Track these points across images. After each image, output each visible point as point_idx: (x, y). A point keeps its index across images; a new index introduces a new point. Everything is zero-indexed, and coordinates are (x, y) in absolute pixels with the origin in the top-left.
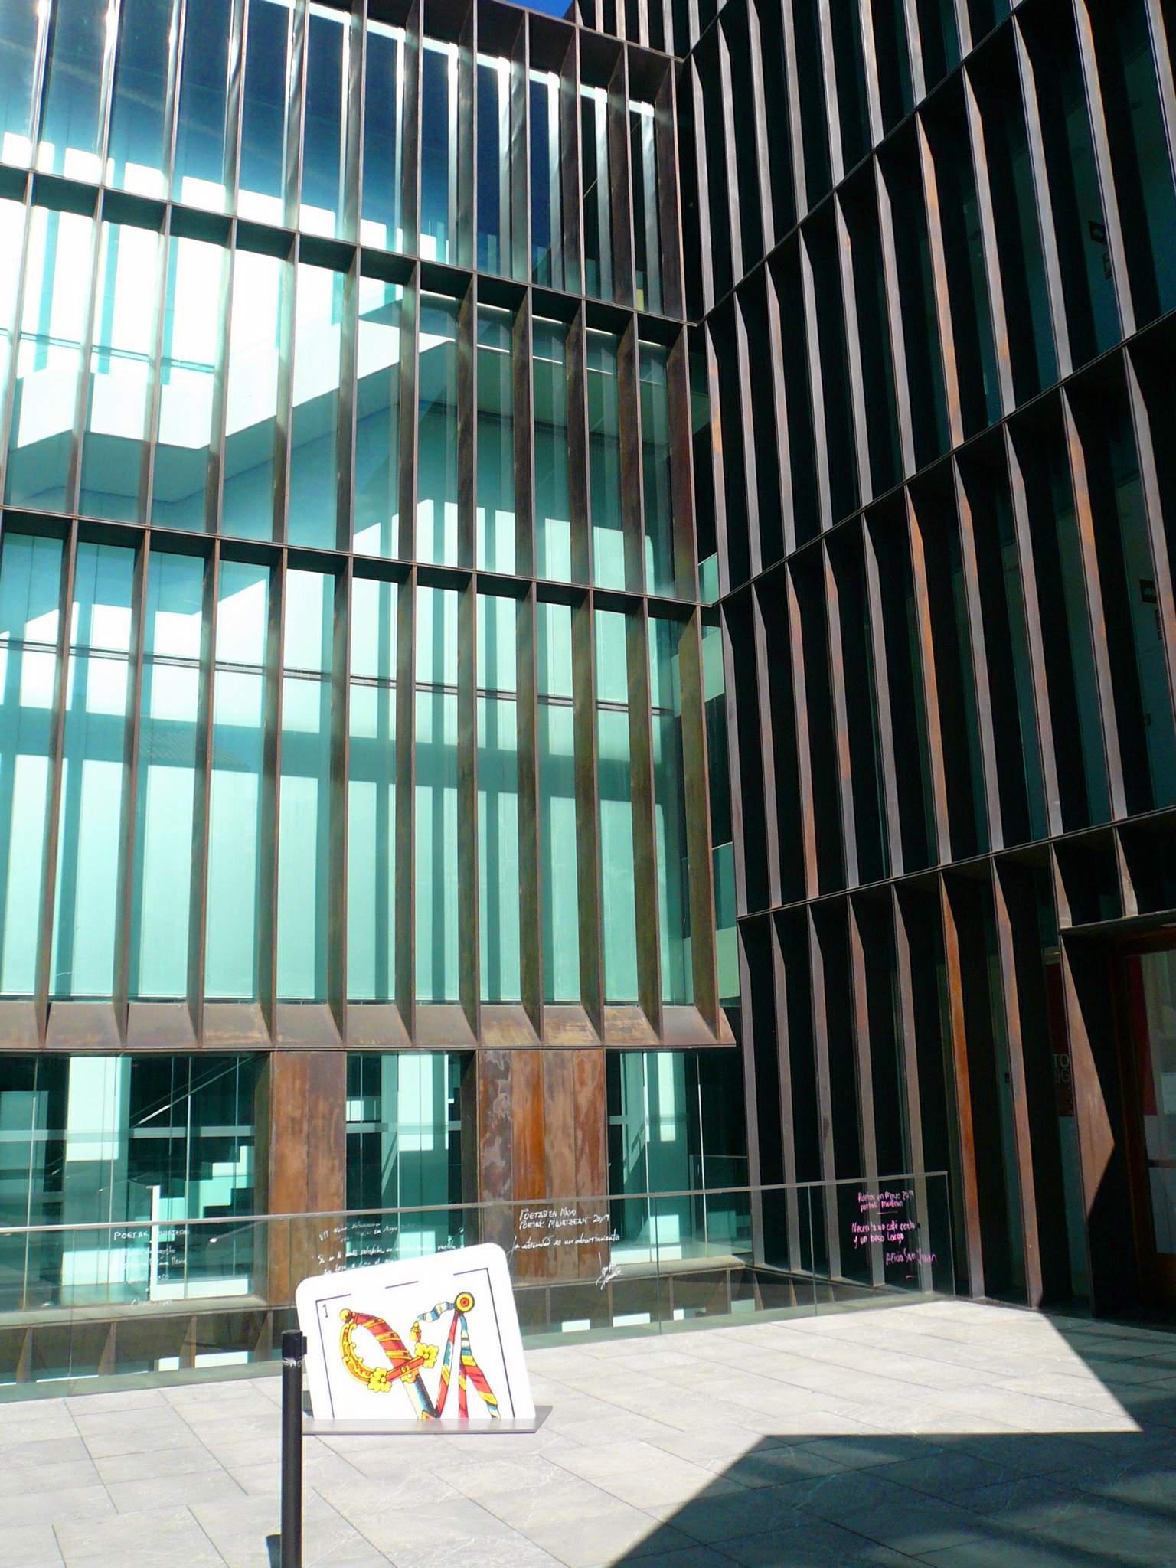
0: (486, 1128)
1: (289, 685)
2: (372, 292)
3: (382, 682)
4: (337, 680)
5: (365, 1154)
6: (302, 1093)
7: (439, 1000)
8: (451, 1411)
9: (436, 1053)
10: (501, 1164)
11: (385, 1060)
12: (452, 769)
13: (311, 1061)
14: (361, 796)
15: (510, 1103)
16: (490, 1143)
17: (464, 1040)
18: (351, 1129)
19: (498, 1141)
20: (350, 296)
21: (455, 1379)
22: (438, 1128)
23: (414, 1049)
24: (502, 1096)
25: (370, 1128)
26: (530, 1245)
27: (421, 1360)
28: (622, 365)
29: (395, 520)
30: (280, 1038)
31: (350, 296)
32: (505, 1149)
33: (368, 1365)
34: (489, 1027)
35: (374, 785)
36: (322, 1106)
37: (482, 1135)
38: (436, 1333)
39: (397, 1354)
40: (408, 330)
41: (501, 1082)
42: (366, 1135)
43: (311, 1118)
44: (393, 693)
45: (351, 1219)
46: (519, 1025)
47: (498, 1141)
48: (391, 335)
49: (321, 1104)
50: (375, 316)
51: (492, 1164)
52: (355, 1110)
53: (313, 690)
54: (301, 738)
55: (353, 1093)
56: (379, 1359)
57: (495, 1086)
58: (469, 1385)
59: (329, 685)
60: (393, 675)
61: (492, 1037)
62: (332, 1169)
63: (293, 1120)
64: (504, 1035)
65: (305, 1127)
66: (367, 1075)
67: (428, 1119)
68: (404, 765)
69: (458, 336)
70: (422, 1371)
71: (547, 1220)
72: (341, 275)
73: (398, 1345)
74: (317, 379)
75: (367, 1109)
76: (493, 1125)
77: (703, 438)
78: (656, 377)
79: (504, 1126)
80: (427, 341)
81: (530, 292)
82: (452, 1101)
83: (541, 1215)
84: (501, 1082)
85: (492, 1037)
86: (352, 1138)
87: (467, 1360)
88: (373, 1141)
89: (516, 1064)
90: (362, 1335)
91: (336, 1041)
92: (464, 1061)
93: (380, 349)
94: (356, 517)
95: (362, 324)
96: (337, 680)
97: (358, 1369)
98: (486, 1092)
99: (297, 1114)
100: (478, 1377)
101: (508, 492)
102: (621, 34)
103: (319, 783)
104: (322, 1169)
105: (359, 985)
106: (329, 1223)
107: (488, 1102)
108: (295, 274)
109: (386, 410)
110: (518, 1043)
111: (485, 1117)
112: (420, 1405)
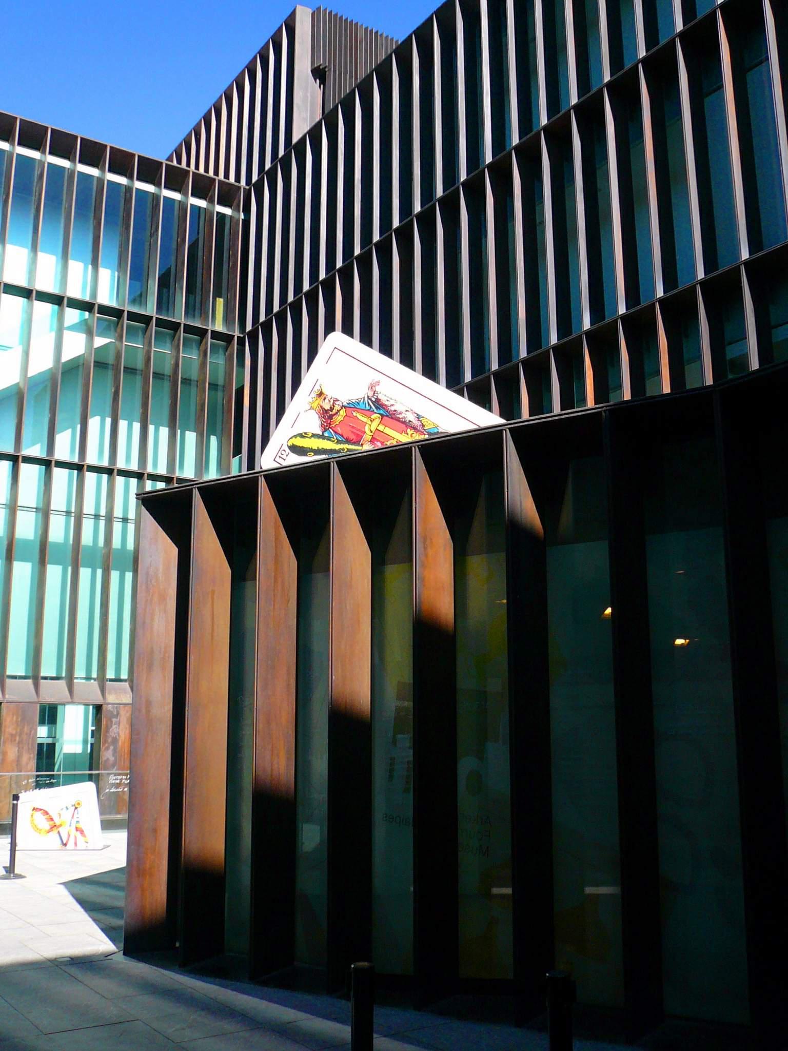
0: (106, 741)
1: (20, 515)
2: (73, 316)
3: (68, 513)
4: (44, 512)
5: (46, 755)
6: (17, 722)
7: (88, 678)
8: (71, 845)
9: (87, 705)
10: (112, 759)
11: (59, 708)
12: (99, 560)
13: (21, 707)
14: (54, 573)
15: (120, 730)
16: (107, 749)
17: (99, 700)
18: (40, 741)
19: (112, 748)
20: (61, 317)
21: (73, 832)
22: (85, 741)
23: (72, 703)
24: (114, 727)
25: (50, 741)
26: (113, 790)
27: (61, 825)
28: (202, 354)
29: (79, 426)
30: (7, 696)
31: (61, 317)
32: (115, 751)
33: (39, 827)
34: (110, 693)
35: (61, 567)
36: (26, 729)
37: (104, 744)
38: (67, 815)
39: (52, 823)
40: (90, 333)
41: (114, 720)
42: (48, 745)
43: (20, 735)
44: (73, 518)
45: (38, 776)
46: (125, 692)
47: (112, 748)
48: (82, 337)
49: (26, 729)
50: (72, 328)
51: (108, 759)
52: (42, 732)
53: (32, 516)
54: (26, 542)
55: (42, 722)
56: (46, 825)
57: (112, 722)
58: (78, 834)
59: (40, 515)
60: (73, 510)
61: (111, 698)
62: (30, 759)
63: (12, 735)
64: (119, 696)
65: (17, 738)
66: (50, 715)
67: (80, 737)
68: (76, 557)
69: (116, 339)
70: (60, 829)
71: (121, 779)
72: (56, 307)
73: (52, 820)
74: (42, 362)
75: (50, 731)
76: (110, 740)
77: (240, 392)
78: (221, 360)
79: (115, 741)
80: (99, 341)
81: (154, 319)
82: (94, 728)
83: (119, 777)
84: (114, 720)
85: (111, 698)
86: (40, 746)
87: (79, 826)
88: (52, 747)
89: (122, 712)
90: (38, 815)
91: (34, 698)
92: (98, 708)
93: (75, 346)
94: (58, 426)
95: (65, 332)
96: (44, 512)
97: (37, 829)
98: (107, 725)
99: (14, 732)
100: (82, 832)
101: (138, 412)
102: (211, 173)
103: (30, 541)
104: (25, 759)
105: (48, 668)
106: (28, 777)
107: (107, 731)
108: (32, 305)
109: (78, 367)
110: (124, 701)
111: (106, 736)
112: (60, 842)
